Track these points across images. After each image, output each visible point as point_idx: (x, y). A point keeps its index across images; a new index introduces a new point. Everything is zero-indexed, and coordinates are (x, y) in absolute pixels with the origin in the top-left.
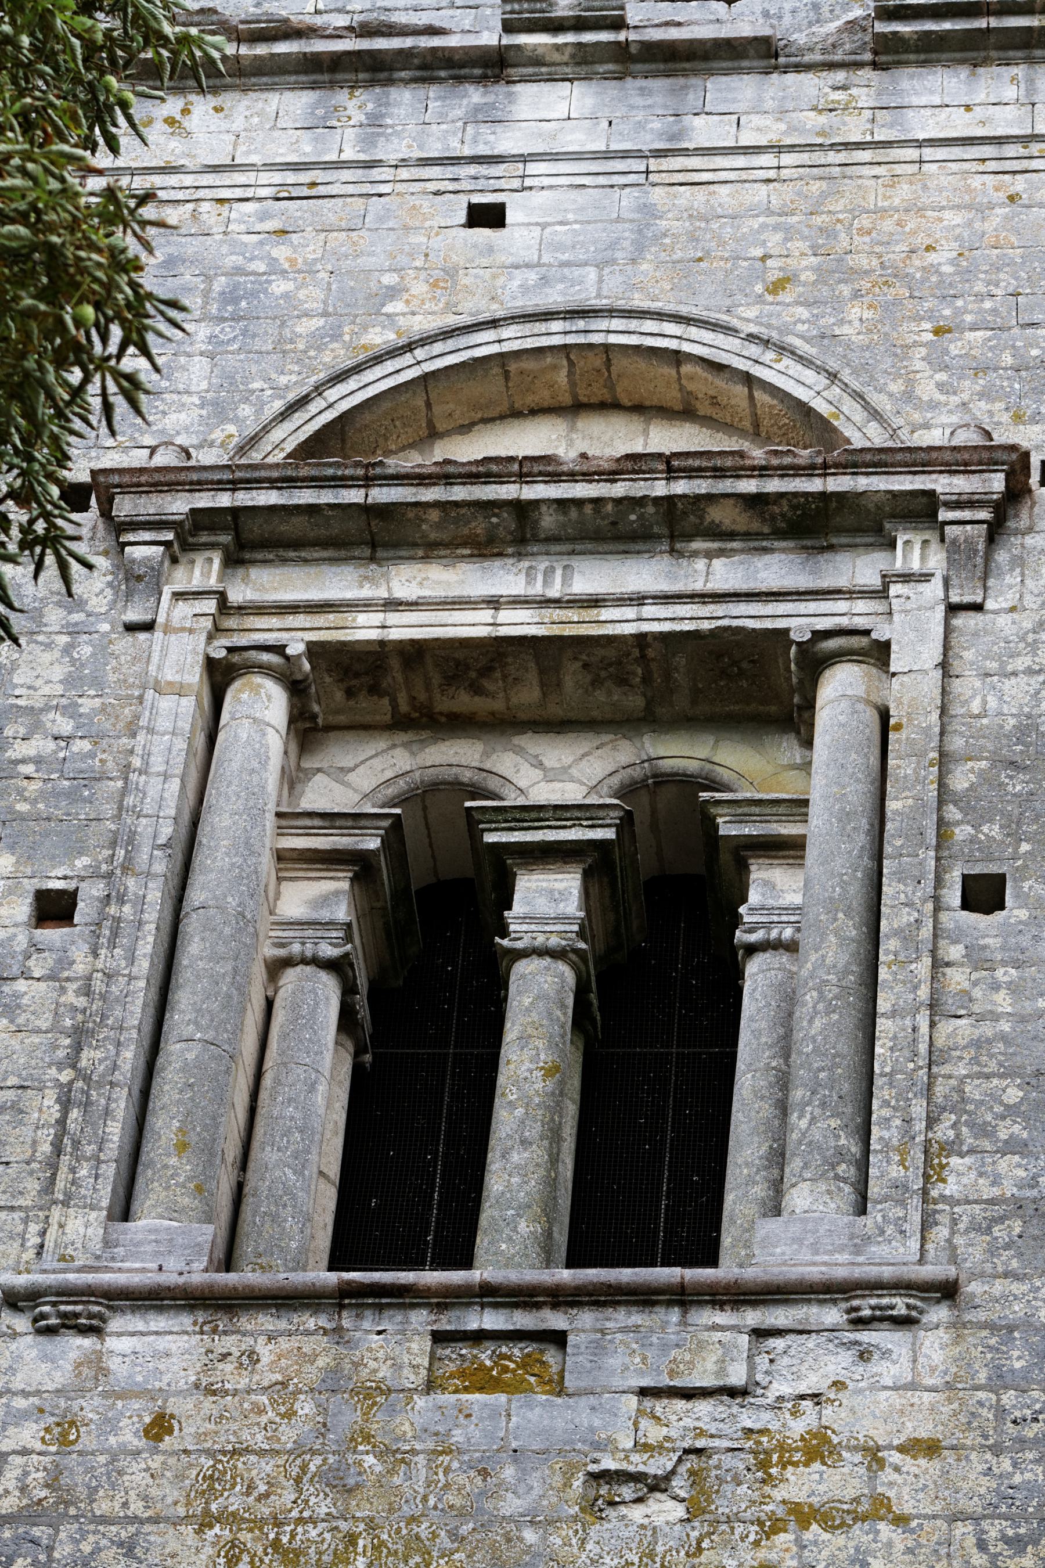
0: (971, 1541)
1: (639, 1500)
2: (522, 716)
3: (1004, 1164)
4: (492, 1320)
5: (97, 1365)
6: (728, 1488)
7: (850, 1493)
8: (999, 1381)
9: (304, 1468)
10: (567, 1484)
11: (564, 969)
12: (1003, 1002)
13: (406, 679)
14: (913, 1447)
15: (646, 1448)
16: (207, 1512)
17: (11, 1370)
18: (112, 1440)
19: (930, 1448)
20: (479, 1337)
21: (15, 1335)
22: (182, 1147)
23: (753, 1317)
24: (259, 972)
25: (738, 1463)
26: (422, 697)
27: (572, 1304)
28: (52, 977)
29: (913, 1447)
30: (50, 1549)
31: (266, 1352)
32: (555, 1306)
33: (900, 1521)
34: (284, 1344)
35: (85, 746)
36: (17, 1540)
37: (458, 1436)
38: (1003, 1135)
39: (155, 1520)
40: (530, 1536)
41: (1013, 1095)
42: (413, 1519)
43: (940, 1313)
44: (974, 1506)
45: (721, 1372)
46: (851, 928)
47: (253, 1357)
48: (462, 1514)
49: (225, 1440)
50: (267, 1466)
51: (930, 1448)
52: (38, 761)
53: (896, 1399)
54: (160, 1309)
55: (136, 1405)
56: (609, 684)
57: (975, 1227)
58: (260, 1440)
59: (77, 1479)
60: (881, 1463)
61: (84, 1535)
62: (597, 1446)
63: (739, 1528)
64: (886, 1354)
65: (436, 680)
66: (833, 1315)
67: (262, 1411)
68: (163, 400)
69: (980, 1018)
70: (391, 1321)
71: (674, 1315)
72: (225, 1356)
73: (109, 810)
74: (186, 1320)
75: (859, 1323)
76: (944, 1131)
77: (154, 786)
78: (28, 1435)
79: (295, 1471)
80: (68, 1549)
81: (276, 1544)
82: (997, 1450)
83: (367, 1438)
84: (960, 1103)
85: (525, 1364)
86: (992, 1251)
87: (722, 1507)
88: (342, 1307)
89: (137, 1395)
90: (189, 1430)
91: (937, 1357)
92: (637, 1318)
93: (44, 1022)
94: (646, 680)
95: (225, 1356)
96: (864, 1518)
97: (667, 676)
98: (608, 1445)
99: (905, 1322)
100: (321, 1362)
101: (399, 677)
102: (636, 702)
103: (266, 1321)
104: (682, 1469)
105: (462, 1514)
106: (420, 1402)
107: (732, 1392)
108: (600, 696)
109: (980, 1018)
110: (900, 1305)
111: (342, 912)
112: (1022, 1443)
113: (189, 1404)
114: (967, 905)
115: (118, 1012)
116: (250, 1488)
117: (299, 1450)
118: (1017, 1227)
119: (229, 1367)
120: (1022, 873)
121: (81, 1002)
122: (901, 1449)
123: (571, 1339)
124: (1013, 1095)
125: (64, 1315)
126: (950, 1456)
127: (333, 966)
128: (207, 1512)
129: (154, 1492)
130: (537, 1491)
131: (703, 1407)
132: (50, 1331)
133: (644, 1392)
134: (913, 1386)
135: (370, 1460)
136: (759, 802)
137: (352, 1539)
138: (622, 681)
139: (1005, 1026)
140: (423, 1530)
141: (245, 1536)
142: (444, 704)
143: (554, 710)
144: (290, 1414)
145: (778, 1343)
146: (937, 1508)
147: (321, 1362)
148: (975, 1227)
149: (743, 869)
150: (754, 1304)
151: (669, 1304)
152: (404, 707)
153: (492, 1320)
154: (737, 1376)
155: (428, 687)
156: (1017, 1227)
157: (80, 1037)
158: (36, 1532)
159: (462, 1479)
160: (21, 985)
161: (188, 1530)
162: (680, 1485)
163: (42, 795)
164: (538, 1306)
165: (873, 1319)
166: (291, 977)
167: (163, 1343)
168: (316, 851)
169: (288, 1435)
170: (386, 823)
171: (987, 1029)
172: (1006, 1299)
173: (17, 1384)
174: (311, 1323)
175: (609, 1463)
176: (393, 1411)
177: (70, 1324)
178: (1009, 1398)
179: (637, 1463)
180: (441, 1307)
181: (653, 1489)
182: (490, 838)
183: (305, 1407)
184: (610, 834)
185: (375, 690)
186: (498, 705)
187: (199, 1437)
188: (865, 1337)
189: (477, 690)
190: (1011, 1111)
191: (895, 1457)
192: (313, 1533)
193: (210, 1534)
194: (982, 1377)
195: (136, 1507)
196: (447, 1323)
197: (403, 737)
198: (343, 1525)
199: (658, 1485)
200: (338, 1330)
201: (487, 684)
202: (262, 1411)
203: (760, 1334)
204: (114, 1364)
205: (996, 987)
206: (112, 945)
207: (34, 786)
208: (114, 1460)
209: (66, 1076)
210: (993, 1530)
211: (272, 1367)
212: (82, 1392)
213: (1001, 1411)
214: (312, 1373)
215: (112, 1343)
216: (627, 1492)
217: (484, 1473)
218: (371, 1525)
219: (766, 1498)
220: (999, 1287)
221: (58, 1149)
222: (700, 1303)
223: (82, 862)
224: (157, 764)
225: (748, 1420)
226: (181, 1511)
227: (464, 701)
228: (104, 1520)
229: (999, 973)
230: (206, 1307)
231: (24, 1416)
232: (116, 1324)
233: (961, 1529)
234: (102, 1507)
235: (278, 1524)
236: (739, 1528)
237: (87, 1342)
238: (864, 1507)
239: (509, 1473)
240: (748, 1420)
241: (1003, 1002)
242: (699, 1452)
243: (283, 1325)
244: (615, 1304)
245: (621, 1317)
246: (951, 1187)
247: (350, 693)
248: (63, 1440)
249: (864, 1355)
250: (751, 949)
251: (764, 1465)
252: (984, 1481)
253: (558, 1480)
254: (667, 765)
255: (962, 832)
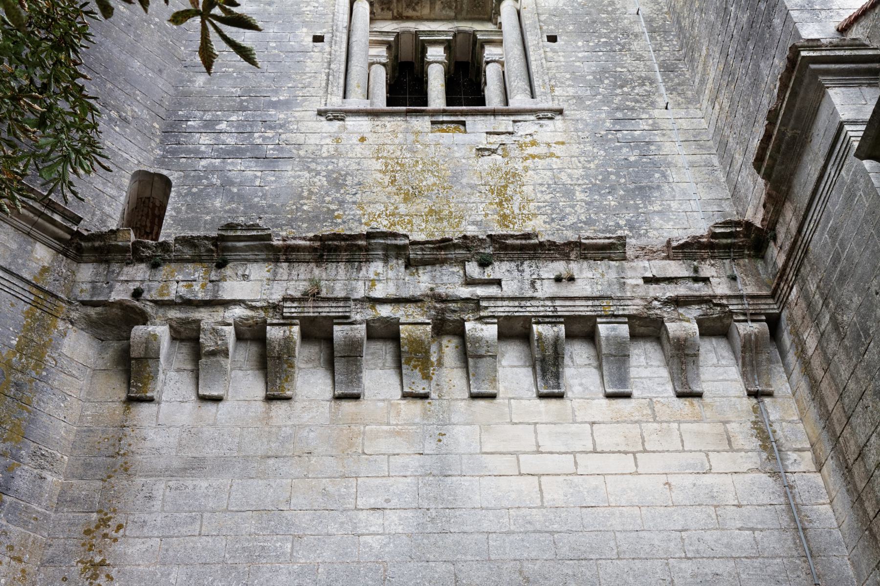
0: (577, 161)
1: (489, 155)
2: (425, 17)
3: (568, 89)
4: (446, 119)
5: (345, 128)
6: (513, 151)
7: (544, 152)
8: (577, 130)
9: (402, 148)
10: (471, 151)
11: (441, 66)
12: (562, 59)
13: (397, 5)
14: (557, 143)
15: (490, 143)
16: (378, 156)
17: (322, 128)
18: (351, 142)
19: (563, 143)
20: (442, 122)
21: (321, 121)
22: (358, 86)
23: (512, 118)
24: (366, 66)
25: (515, 146)
26: (400, 11)
27: (466, 115)
28: (320, 52)
29: (557, 143)
30: (337, 164)
31: (388, 125)
32: (462, 115)
33: (558, 157)
34: (393, 123)
35: (322, 8)
36: (328, 162)
37: (441, 141)
38: (567, 84)
39: (365, 158)
40: (464, 161)
41: (568, 76)
42: (432, 158)
43: (559, 117)
44: (576, 154)
45: (506, 129)
46: (520, 47)
47: (385, 126)
48: (445, 157)
49: (380, 141)
50: (393, 147)
51: (563, 143)
52: (310, 11)
53: (552, 134)
54: (359, 116)
55: (356, 135)
56: (447, 8)
57: (564, 101)
58: (389, 142)
59: (342, 148)
60: (551, 146)
61: (346, 161)
62: (477, 143)
63: (517, 159)
64: (547, 125)
65: (404, 6)
66: (533, 118)
67: (389, 136)
68: (310, 58)
69: (557, 62)
70: (420, 119)
71: (492, 117)
72: (377, 126)
73: (330, 20)
74: (366, 118)
75: (540, 119)
76: (553, 83)
77: (341, 16)
78: (329, 141)
79: (400, 148)
80: (342, 164)
81: (397, 163)
82: (579, 143)
83: (418, 142)
84: (555, 78)
85: (455, 128)
86: (570, 105)
87: (512, 155)
88: (407, 115)
89: (356, 133)
90: (370, 140)
91: (560, 126)
92: (483, 118)
93: (320, 60)
94: (456, 8)
95: (377, 126)
96: (549, 157)
97: (462, 7)
98: (481, 143)
99: (551, 118)
100: (403, 127)
101: (395, 5)
102: (452, 14)
103: (387, 119)
104: (500, 148)
105: (445, 157)
106: (430, 135)
107: (510, 133)
108: (444, 12)
109: (557, 62)
110: (550, 115)
111: (385, 54)
112: (585, 142)
113: (370, 135)
114: (548, 41)
115: (339, 58)
116: (389, 152)
117: (400, 144)
118: (575, 101)
119: (379, 128)
120: (561, 35)
121: (329, 56)
122: (555, 143)
123: (467, 122)
124: (568, 76)
125: (334, 116)
126: (568, 145)
127: (384, 65)
128: (378, 156)
129: (363, 152)
130: (464, 152)
131: (503, 136)
132: (331, 120)
133: (487, 133)
134: (555, 131)
135: (419, 146)
136: (487, 31)
137: (417, 162)
138: (450, 8)
139: (563, 64)
140: (436, 159)
141: (389, 161)
142: (405, 14)
143: (433, 16)
144: (397, 137)
145: (517, 124)
146: (567, 155)
147: (403, 127)
148: (564, 101)
149: (482, 47)
150: (512, 115)
151: (491, 115)
152: (395, 14)
153: (446, 119)
154: (510, 129)
155: (402, 8)
156: (575, 101)
157: (329, 63)
158: (333, 160)
159: (444, 150)
160: (312, 53)
161: (374, 160)
162: (500, 151)
163: (312, 17)
164: (457, 115)
165: (543, 118)
166: (374, 67)
167: (361, 123)
168: (378, 40)
169: (397, 141)
170: (395, 34)
171: (559, 64)
172: (575, 115)
173: (323, 131)
174: (399, 119)
175: (481, 146)
176: (423, 136)
177: (336, 118)
178: (580, 134)
179: (488, 146)
180: (432, 116)
181: (493, 153)
182: (421, 38)
183: (400, 135)
184: (451, 38)
185: (389, 9)
186: (419, 14)
187: (373, 141)
188: (541, 122)
189: (414, 10)
190: (568, 79)
191: (554, 145)
192: (407, 161)
193: (380, 161)
194: (572, 129)
195: (359, 155)
196: (434, 119)
197: (394, 22)
198: (415, 159)
199: (494, 151)
200: (406, 120)
201: (417, 8)
202: (389, 136)
203: (514, 122)
204: (348, 127)
205: (559, 56)
206: (335, 45)
207: (310, 16)
208: (351, 146)
209: (327, 71)
210: (582, 159)
211: (390, 128)
212: (341, 132)
213: (579, 136)
214: (401, 129)
215: (346, 123)
216: (486, 153)
217: (449, 149)
218: (422, 159)
219: (522, 153)
220: (573, 112)
221: (327, 84)
222: (499, 115)
223: (324, 30)
224: (341, 12)
225: (514, 138)
226: (371, 156)
227: (410, 13)
228: (351, 158)
229: (560, 53)
230: (371, 115)
231: (326, 137)
232: (347, 119)
233: (573, 159)
234: (350, 155)
235: (397, 158)
236: (517, 159)
237: (341, 122)
238: (548, 155)
239: (456, 148)
240: (514, 138)
241: (562, 59)
242: (504, 144)
243: (392, 119)
244: (477, 115)
245: (478, 118)
246: (556, 93)
247: (382, 9)
248: (337, 142)
249: (541, 126)
250: (487, 63)
251: (521, 147)
252: (578, 150)
253: (469, 150)
254: (461, 29)
255: (545, 28)
